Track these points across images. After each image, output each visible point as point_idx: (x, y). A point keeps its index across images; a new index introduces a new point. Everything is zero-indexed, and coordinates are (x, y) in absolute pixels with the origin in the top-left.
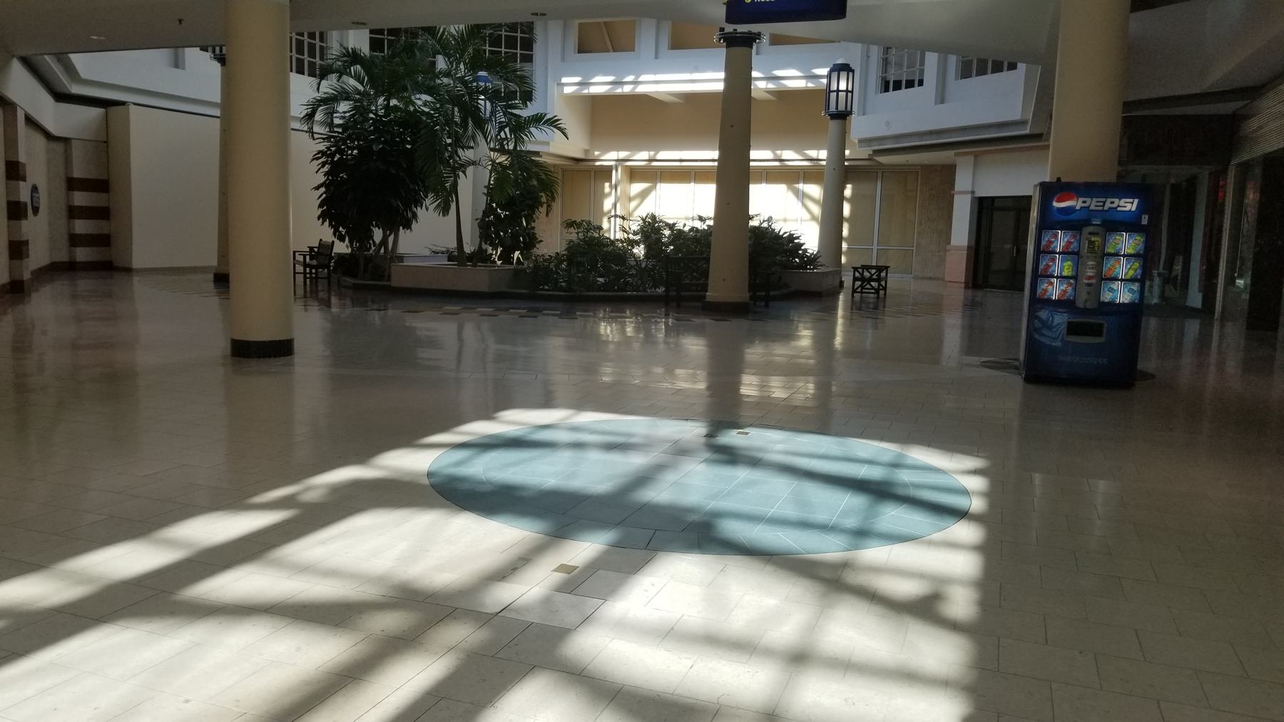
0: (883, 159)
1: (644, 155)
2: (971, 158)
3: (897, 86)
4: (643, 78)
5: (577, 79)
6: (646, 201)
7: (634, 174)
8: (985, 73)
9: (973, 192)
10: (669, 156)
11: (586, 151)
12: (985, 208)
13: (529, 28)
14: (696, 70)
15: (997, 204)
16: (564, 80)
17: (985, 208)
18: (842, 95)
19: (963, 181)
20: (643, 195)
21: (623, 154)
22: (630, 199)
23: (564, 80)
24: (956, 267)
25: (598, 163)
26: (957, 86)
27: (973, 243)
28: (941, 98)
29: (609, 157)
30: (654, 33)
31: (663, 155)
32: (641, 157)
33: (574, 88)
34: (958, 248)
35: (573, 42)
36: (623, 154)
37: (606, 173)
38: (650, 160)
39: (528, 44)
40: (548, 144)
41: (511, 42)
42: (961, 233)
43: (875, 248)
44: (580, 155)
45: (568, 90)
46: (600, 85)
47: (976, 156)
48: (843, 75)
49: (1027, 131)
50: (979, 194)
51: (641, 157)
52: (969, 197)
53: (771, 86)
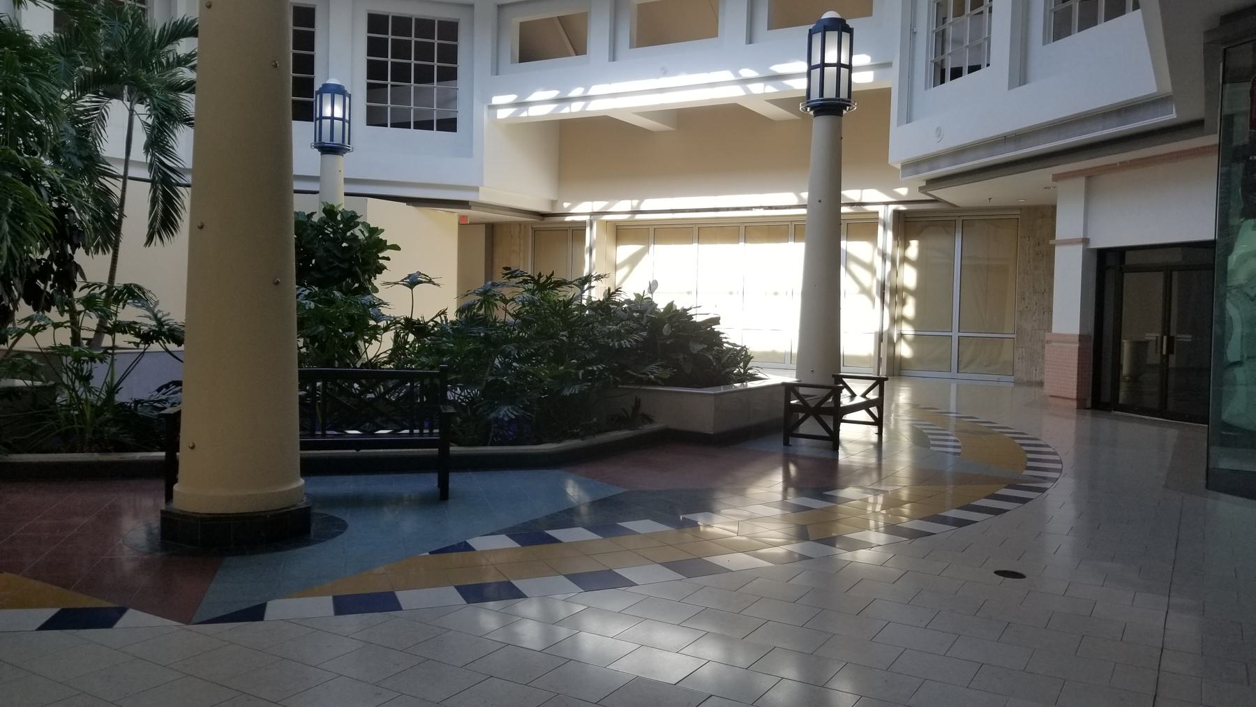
0: (949, 194)
1: (625, 205)
2: (1081, 182)
3: (957, 73)
4: (595, 90)
5: (511, 98)
6: (637, 269)
7: (621, 233)
8: (1094, 22)
9: (1085, 241)
10: (660, 204)
11: (553, 203)
12: (1108, 267)
13: (450, 29)
14: (665, 72)
15: (1130, 259)
16: (496, 100)
17: (1108, 267)
18: (830, 72)
19: (1068, 223)
20: (633, 261)
21: (598, 206)
22: (616, 268)
23: (496, 100)
24: (1063, 372)
25: (568, 219)
26: (1043, 53)
27: (1091, 330)
28: (1020, 75)
29: (581, 209)
30: (1083, 194)
31: (648, 204)
32: (622, 207)
33: (511, 111)
34: (1063, 339)
35: (511, 43)
36: (598, 206)
37: (578, 231)
38: (634, 212)
39: (450, 54)
40: (476, 189)
41: (401, 49)
42: (1068, 312)
43: (955, 334)
44: (544, 208)
45: (503, 114)
46: (542, 105)
47: (1090, 176)
48: (832, 37)
49: (1170, 116)
50: (1100, 242)
51: (622, 207)
52: (1079, 249)
53: (770, 89)
